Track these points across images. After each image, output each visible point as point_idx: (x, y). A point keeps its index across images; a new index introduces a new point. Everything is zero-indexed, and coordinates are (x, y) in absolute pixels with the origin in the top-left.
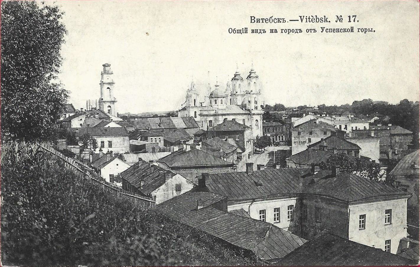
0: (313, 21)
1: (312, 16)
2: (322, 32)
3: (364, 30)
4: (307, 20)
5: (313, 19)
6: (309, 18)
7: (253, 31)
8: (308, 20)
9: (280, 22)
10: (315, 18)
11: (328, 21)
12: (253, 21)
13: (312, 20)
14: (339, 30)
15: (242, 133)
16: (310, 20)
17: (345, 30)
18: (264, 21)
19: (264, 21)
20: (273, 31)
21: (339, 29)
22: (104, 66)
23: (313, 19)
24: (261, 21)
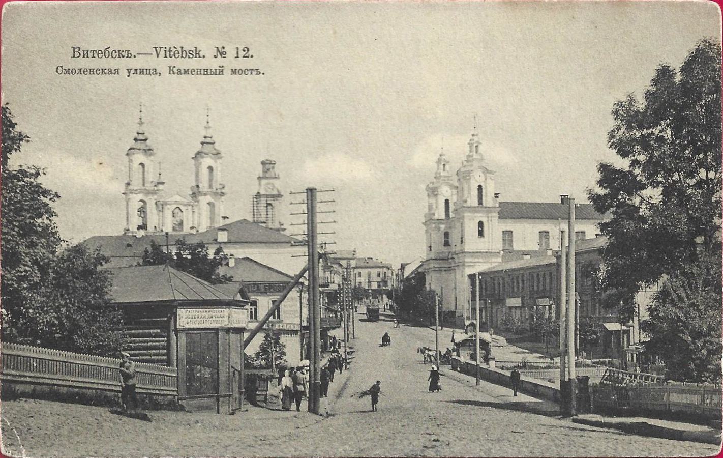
0: (177, 56)
1: (175, 48)
2: (128, 76)
3: (95, 73)
4: (166, 55)
5: (176, 52)
6: (170, 51)
7: (234, 72)
8: (168, 53)
9: (123, 57)
10: (180, 50)
11: (201, 55)
12: (77, 54)
13: (174, 54)
14: (70, 71)
15: (21, 333)
16: (172, 53)
17: (206, 71)
18: (96, 55)
19: (96, 55)
20: (93, 72)
21: (93, 69)
22: (263, 163)
23: (176, 52)
24: (90, 55)
